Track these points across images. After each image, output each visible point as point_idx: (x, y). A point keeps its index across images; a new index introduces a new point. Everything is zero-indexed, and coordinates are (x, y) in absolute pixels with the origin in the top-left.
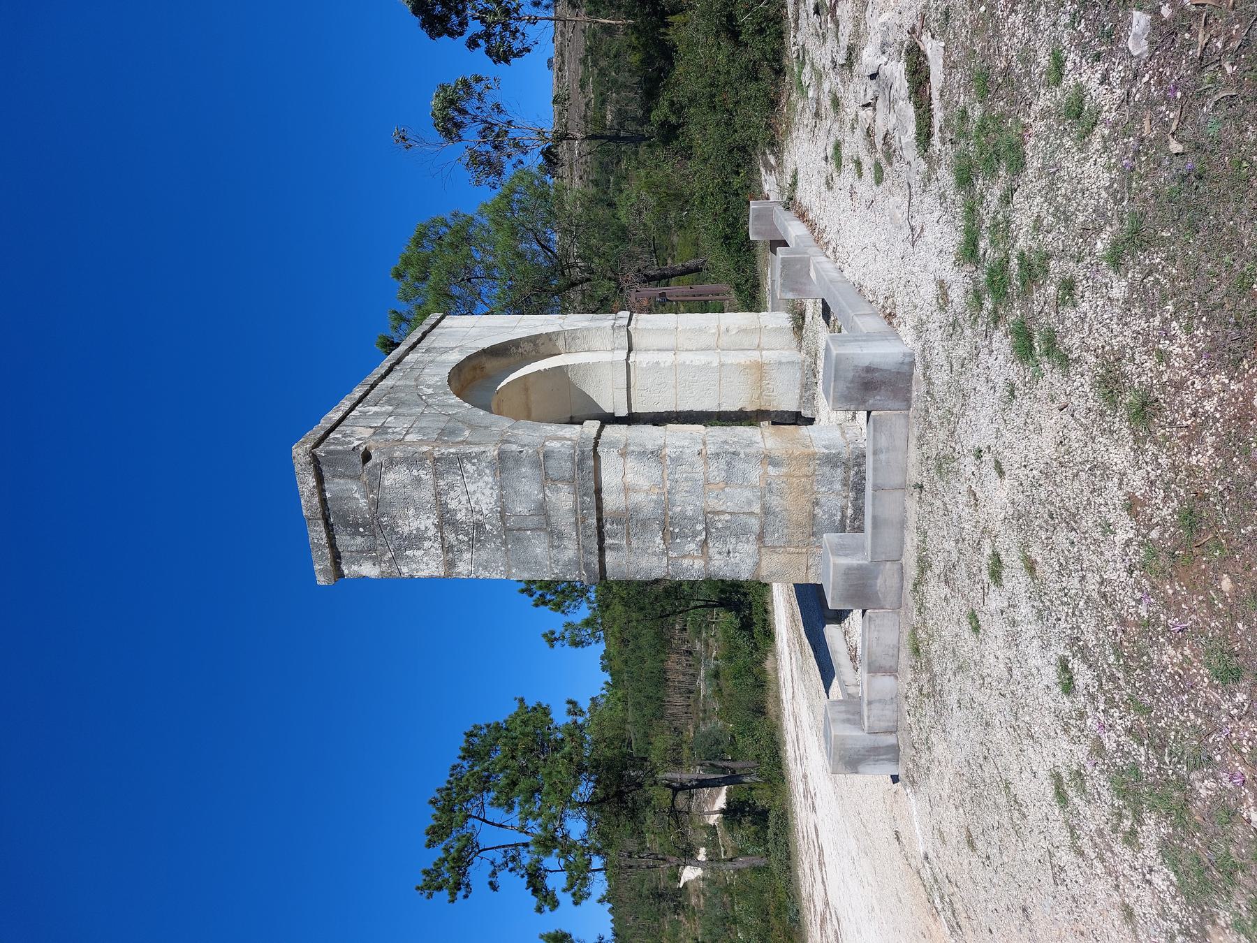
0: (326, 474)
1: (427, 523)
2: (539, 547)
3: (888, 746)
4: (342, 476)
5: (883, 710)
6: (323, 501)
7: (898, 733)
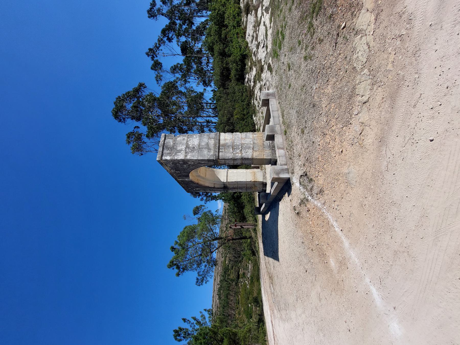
0: (166, 138)
1: (183, 147)
2: (205, 152)
3: (285, 169)
4: (170, 138)
5: (282, 158)
6: (164, 143)
7: (287, 165)
